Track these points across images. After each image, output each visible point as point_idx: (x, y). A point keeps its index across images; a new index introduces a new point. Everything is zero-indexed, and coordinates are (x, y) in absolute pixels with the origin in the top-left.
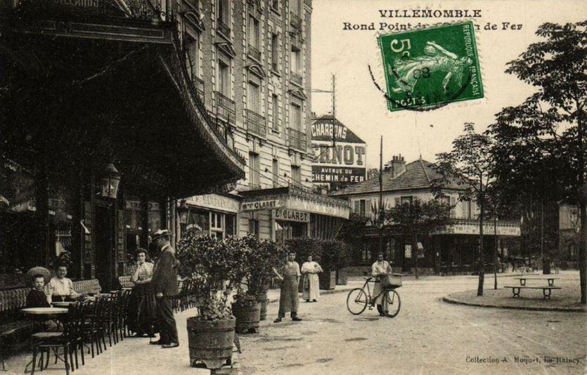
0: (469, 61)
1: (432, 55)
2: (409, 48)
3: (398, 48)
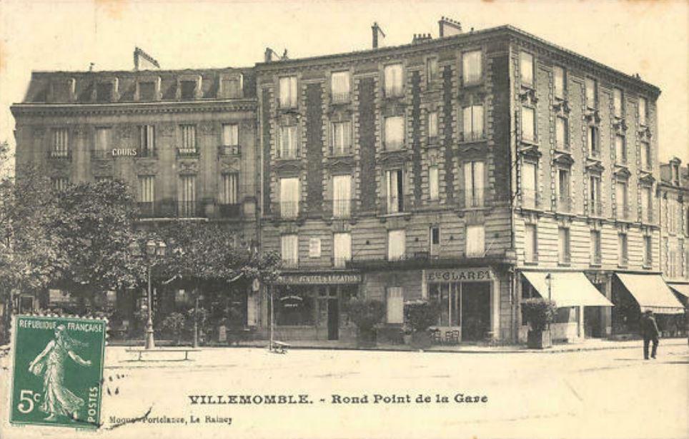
0: (60, 328)
1: (45, 368)
2: (31, 392)
3: (29, 405)
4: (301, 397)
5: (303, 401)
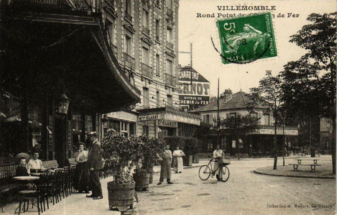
1: (247, 32)
2: (235, 27)
4: (272, 7)
5: (238, 9)
